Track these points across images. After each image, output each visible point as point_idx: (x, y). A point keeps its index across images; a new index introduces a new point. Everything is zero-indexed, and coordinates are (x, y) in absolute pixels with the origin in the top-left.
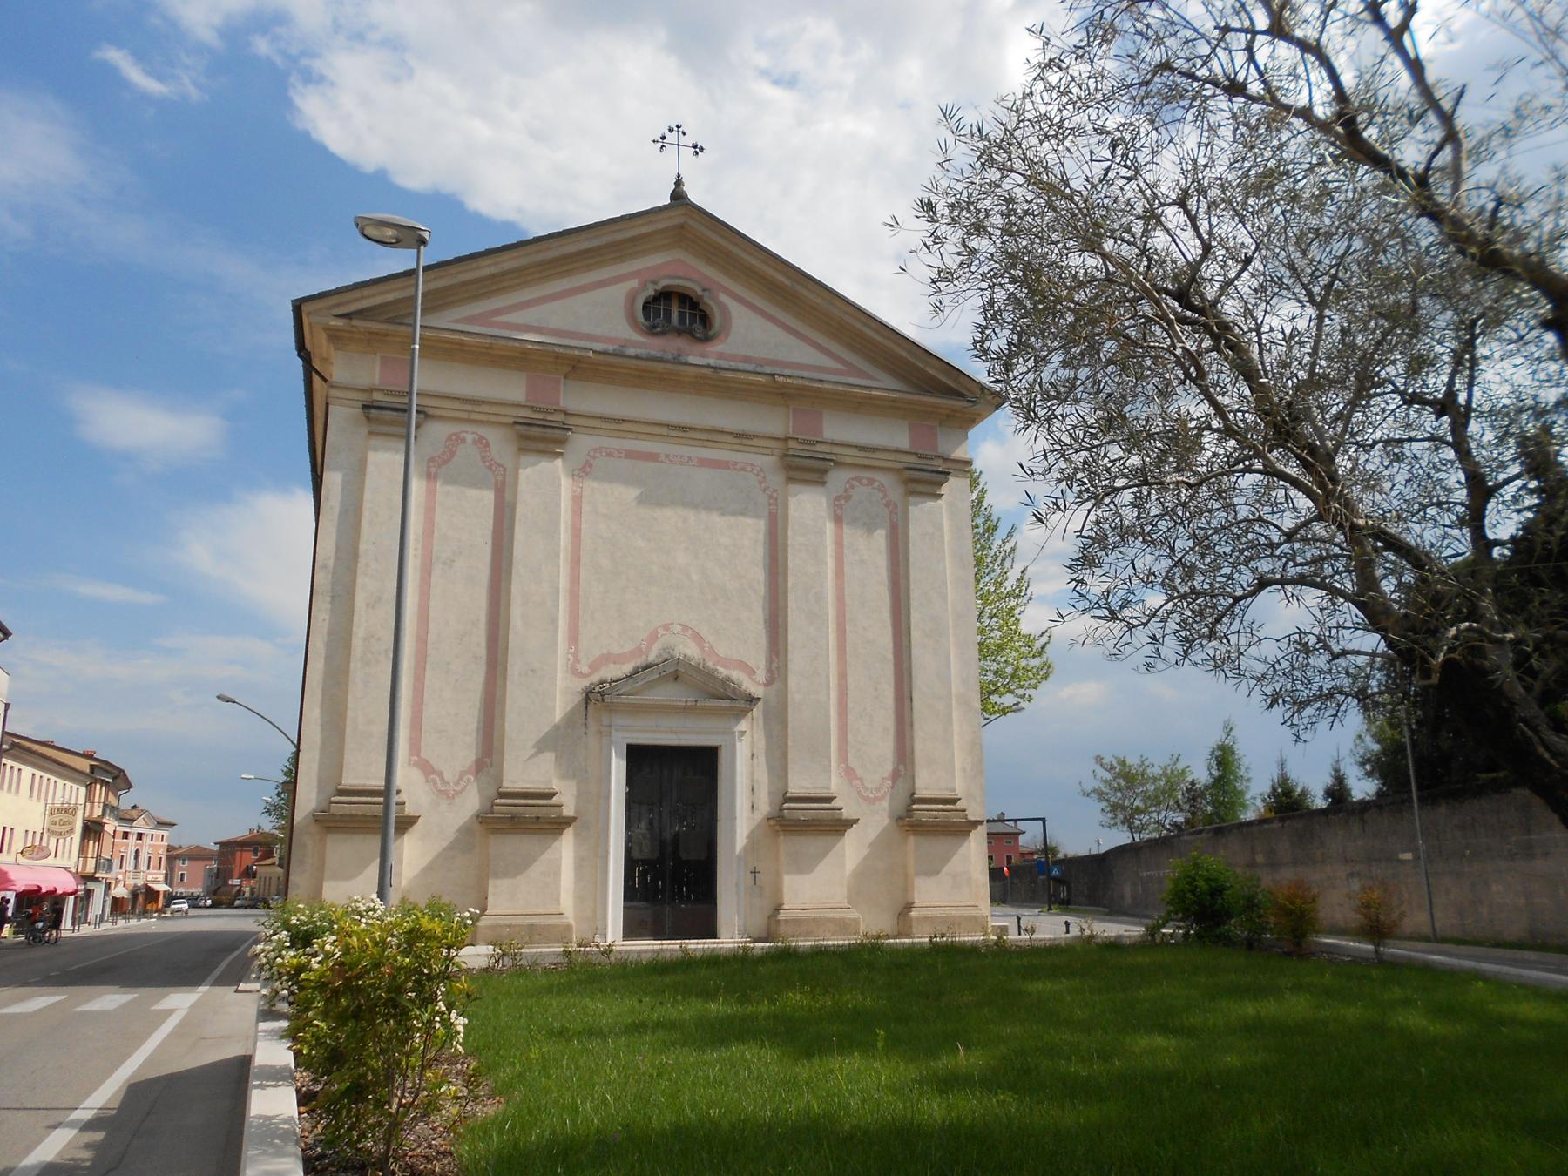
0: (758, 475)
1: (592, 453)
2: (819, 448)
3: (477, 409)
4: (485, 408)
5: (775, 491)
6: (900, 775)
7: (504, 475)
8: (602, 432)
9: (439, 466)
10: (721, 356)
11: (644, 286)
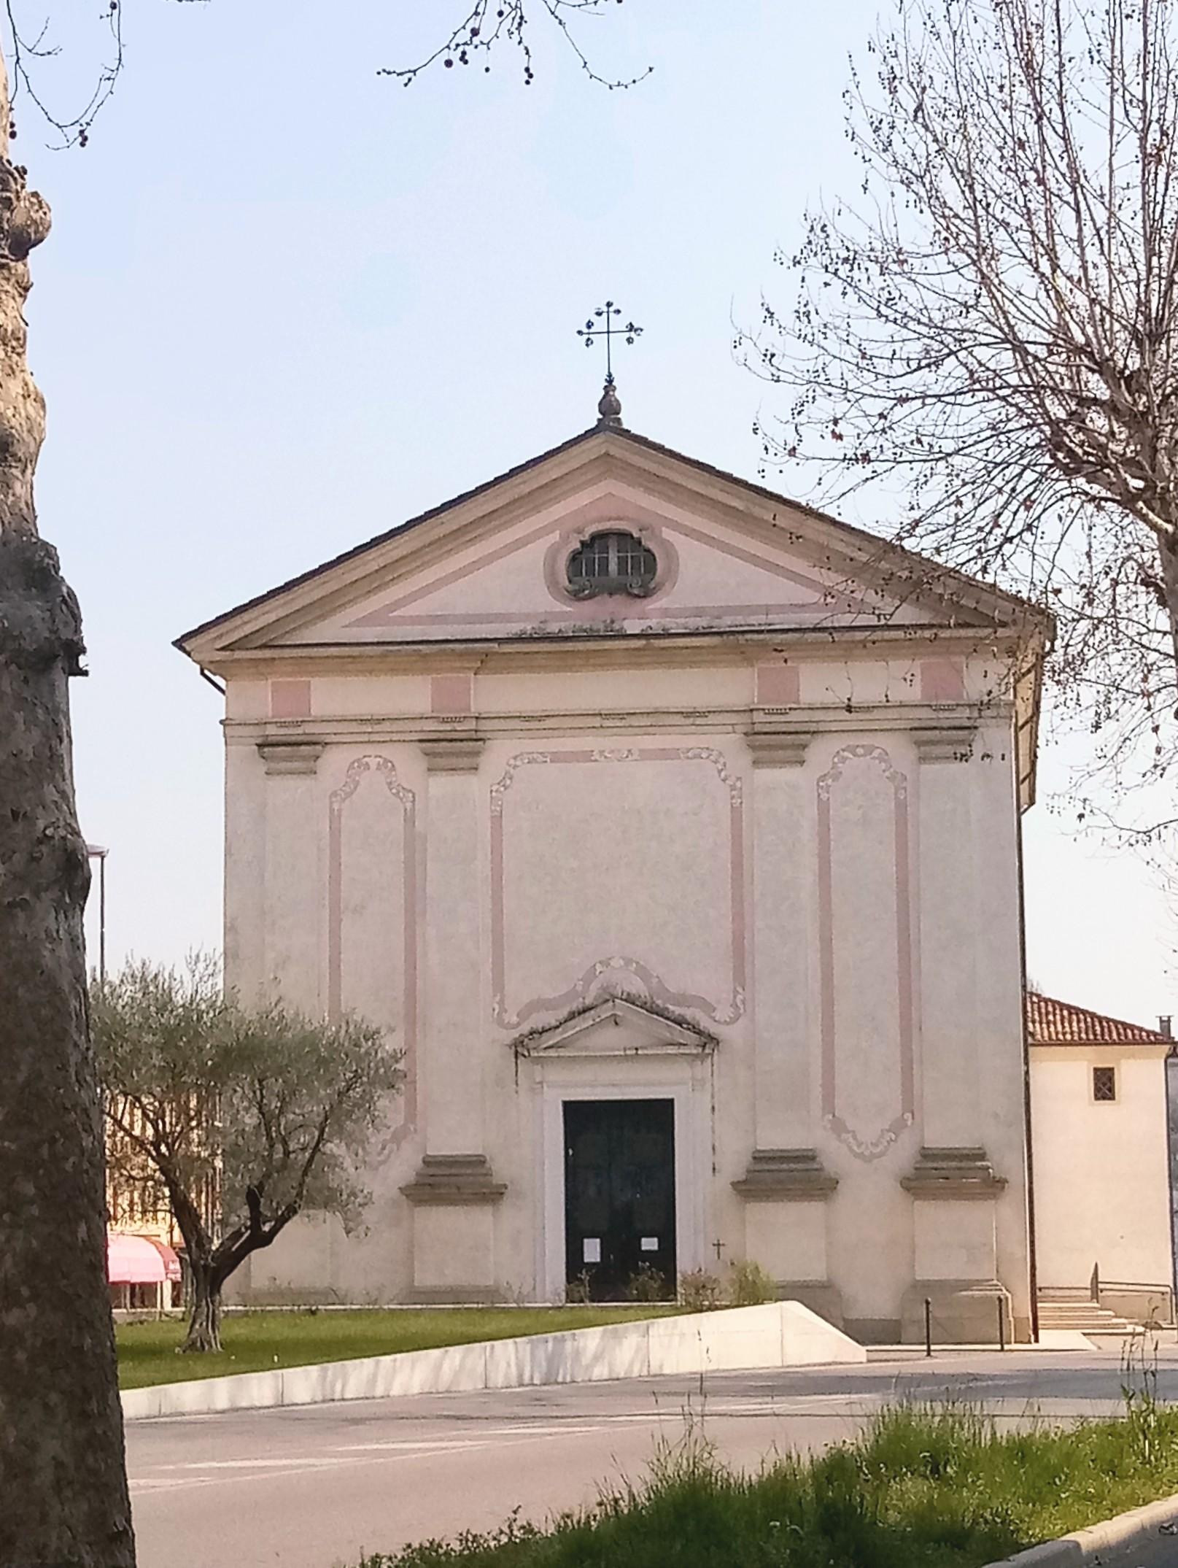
0: (716, 762)
1: (512, 762)
2: (793, 716)
3: (377, 728)
4: (386, 726)
5: (739, 779)
6: (906, 1126)
7: (413, 801)
8: (521, 734)
9: (344, 800)
10: (665, 613)
11: (565, 539)
